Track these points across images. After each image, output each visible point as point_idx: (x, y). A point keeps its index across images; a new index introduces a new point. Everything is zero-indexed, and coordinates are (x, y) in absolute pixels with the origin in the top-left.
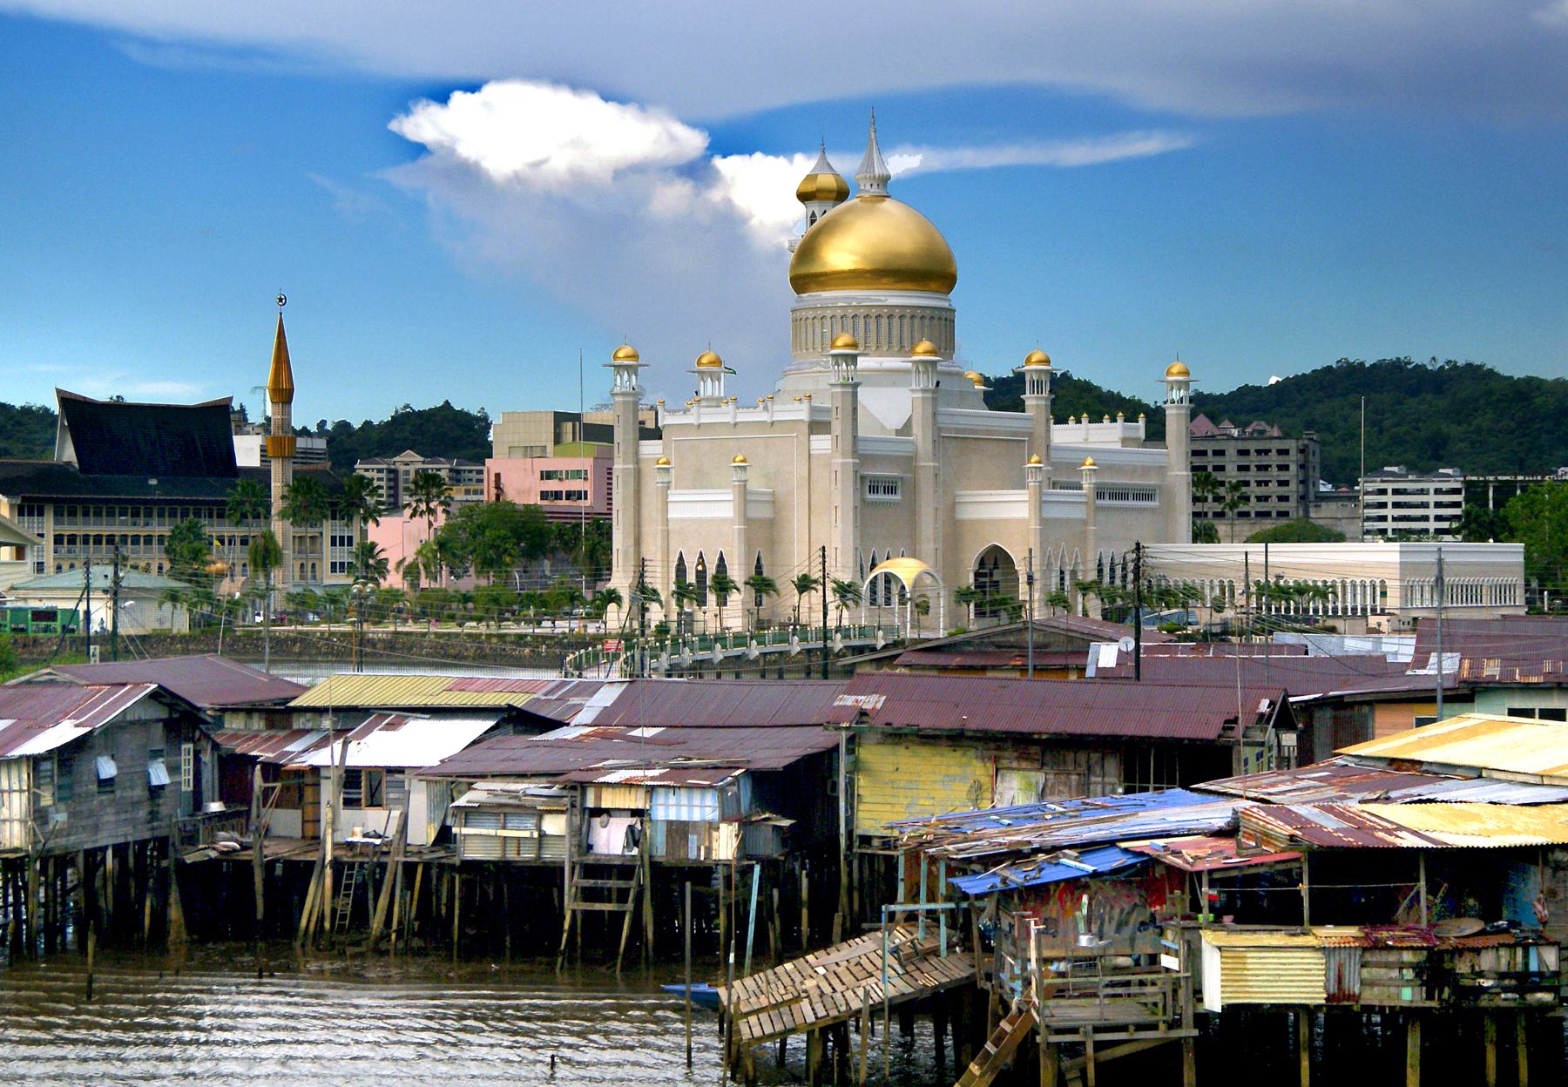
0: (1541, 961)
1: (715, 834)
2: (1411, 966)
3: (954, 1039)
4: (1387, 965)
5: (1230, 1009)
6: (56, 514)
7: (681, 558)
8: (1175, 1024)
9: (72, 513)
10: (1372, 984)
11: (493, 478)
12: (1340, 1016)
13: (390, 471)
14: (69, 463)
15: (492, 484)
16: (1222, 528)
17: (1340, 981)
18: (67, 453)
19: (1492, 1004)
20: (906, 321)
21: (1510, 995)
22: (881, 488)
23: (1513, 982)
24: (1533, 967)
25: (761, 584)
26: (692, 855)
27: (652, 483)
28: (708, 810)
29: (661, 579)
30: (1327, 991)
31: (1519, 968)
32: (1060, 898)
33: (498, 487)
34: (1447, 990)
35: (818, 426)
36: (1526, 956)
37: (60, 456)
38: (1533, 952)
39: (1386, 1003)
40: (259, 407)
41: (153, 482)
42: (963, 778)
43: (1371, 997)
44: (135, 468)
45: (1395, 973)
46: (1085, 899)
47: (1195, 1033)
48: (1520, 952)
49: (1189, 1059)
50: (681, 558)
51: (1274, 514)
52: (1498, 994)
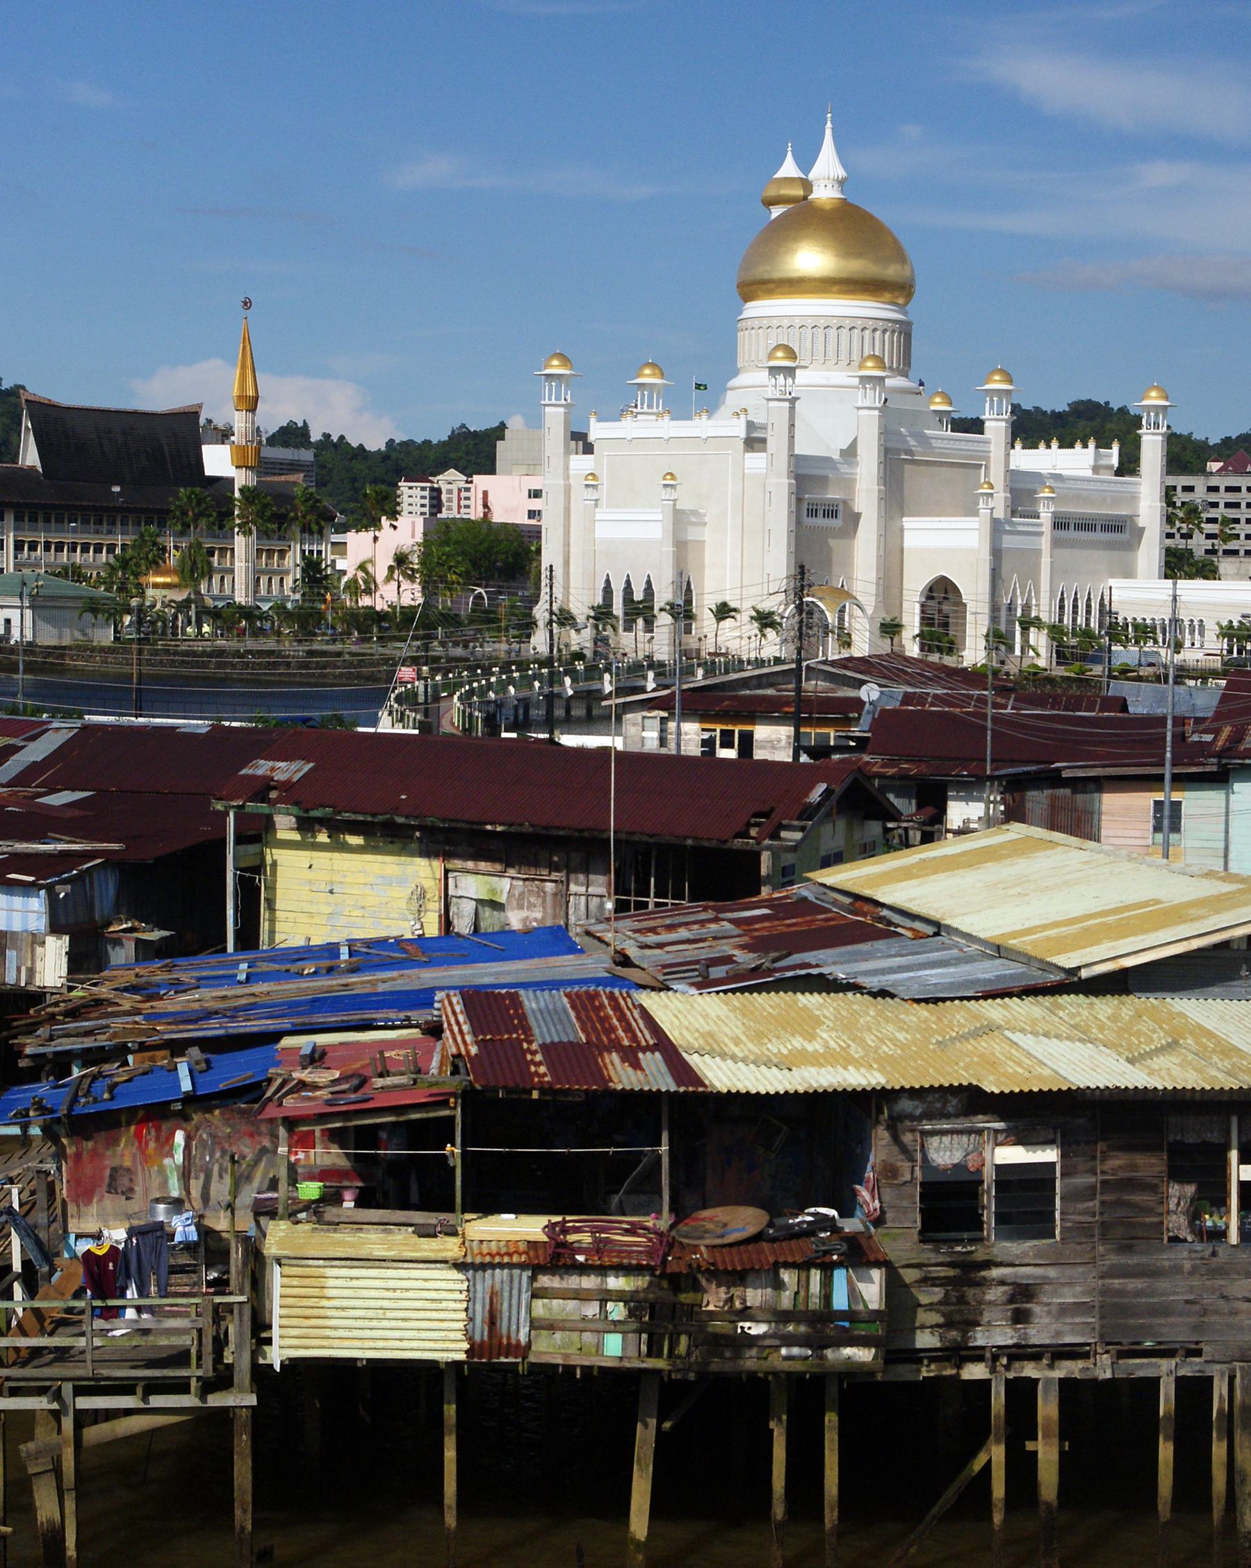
0: (853, 1294)
1: (39, 950)
2: (620, 1296)
3: (671, 1145)
4: (580, 1296)
5: (292, 1365)
6: (16, 520)
7: (608, 582)
8: (222, 1380)
9: (33, 519)
10: (551, 1326)
11: (480, 496)
12: (493, 1388)
13: (432, 489)
14: (33, 468)
15: (480, 502)
16: (1226, 565)
17: (492, 1319)
18: (30, 456)
19: (765, 1366)
20: (832, 332)
21: (796, 1351)
22: (816, 509)
23: (803, 1329)
24: (840, 1301)
25: (683, 613)
26: (10, 978)
27: (580, 498)
28: (33, 916)
29: (580, 607)
30: (470, 1339)
31: (815, 1303)
32: (138, 1135)
33: (485, 505)
34: (684, 1340)
35: (754, 442)
36: (827, 1284)
37: (24, 459)
38: (840, 1276)
39: (576, 1360)
40: (220, 409)
41: (116, 489)
42: (402, 881)
43: (550, 1349)
44: (124, 472)
45: (592, 1309)
46: (179, 1137)
47: (252, 1400)
48: (816, 1276)
49: (243, 1442)
50: (608, 582)
51: (1242, 553)
52: (778, 1348)
